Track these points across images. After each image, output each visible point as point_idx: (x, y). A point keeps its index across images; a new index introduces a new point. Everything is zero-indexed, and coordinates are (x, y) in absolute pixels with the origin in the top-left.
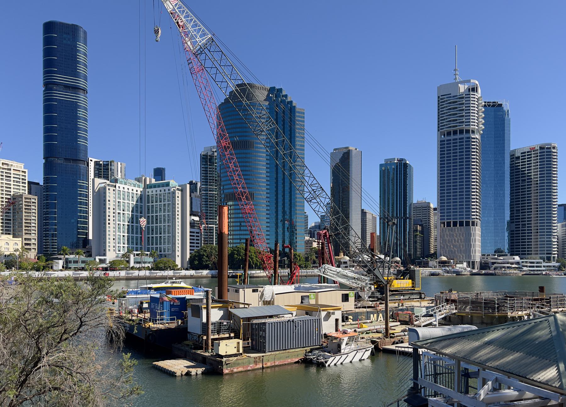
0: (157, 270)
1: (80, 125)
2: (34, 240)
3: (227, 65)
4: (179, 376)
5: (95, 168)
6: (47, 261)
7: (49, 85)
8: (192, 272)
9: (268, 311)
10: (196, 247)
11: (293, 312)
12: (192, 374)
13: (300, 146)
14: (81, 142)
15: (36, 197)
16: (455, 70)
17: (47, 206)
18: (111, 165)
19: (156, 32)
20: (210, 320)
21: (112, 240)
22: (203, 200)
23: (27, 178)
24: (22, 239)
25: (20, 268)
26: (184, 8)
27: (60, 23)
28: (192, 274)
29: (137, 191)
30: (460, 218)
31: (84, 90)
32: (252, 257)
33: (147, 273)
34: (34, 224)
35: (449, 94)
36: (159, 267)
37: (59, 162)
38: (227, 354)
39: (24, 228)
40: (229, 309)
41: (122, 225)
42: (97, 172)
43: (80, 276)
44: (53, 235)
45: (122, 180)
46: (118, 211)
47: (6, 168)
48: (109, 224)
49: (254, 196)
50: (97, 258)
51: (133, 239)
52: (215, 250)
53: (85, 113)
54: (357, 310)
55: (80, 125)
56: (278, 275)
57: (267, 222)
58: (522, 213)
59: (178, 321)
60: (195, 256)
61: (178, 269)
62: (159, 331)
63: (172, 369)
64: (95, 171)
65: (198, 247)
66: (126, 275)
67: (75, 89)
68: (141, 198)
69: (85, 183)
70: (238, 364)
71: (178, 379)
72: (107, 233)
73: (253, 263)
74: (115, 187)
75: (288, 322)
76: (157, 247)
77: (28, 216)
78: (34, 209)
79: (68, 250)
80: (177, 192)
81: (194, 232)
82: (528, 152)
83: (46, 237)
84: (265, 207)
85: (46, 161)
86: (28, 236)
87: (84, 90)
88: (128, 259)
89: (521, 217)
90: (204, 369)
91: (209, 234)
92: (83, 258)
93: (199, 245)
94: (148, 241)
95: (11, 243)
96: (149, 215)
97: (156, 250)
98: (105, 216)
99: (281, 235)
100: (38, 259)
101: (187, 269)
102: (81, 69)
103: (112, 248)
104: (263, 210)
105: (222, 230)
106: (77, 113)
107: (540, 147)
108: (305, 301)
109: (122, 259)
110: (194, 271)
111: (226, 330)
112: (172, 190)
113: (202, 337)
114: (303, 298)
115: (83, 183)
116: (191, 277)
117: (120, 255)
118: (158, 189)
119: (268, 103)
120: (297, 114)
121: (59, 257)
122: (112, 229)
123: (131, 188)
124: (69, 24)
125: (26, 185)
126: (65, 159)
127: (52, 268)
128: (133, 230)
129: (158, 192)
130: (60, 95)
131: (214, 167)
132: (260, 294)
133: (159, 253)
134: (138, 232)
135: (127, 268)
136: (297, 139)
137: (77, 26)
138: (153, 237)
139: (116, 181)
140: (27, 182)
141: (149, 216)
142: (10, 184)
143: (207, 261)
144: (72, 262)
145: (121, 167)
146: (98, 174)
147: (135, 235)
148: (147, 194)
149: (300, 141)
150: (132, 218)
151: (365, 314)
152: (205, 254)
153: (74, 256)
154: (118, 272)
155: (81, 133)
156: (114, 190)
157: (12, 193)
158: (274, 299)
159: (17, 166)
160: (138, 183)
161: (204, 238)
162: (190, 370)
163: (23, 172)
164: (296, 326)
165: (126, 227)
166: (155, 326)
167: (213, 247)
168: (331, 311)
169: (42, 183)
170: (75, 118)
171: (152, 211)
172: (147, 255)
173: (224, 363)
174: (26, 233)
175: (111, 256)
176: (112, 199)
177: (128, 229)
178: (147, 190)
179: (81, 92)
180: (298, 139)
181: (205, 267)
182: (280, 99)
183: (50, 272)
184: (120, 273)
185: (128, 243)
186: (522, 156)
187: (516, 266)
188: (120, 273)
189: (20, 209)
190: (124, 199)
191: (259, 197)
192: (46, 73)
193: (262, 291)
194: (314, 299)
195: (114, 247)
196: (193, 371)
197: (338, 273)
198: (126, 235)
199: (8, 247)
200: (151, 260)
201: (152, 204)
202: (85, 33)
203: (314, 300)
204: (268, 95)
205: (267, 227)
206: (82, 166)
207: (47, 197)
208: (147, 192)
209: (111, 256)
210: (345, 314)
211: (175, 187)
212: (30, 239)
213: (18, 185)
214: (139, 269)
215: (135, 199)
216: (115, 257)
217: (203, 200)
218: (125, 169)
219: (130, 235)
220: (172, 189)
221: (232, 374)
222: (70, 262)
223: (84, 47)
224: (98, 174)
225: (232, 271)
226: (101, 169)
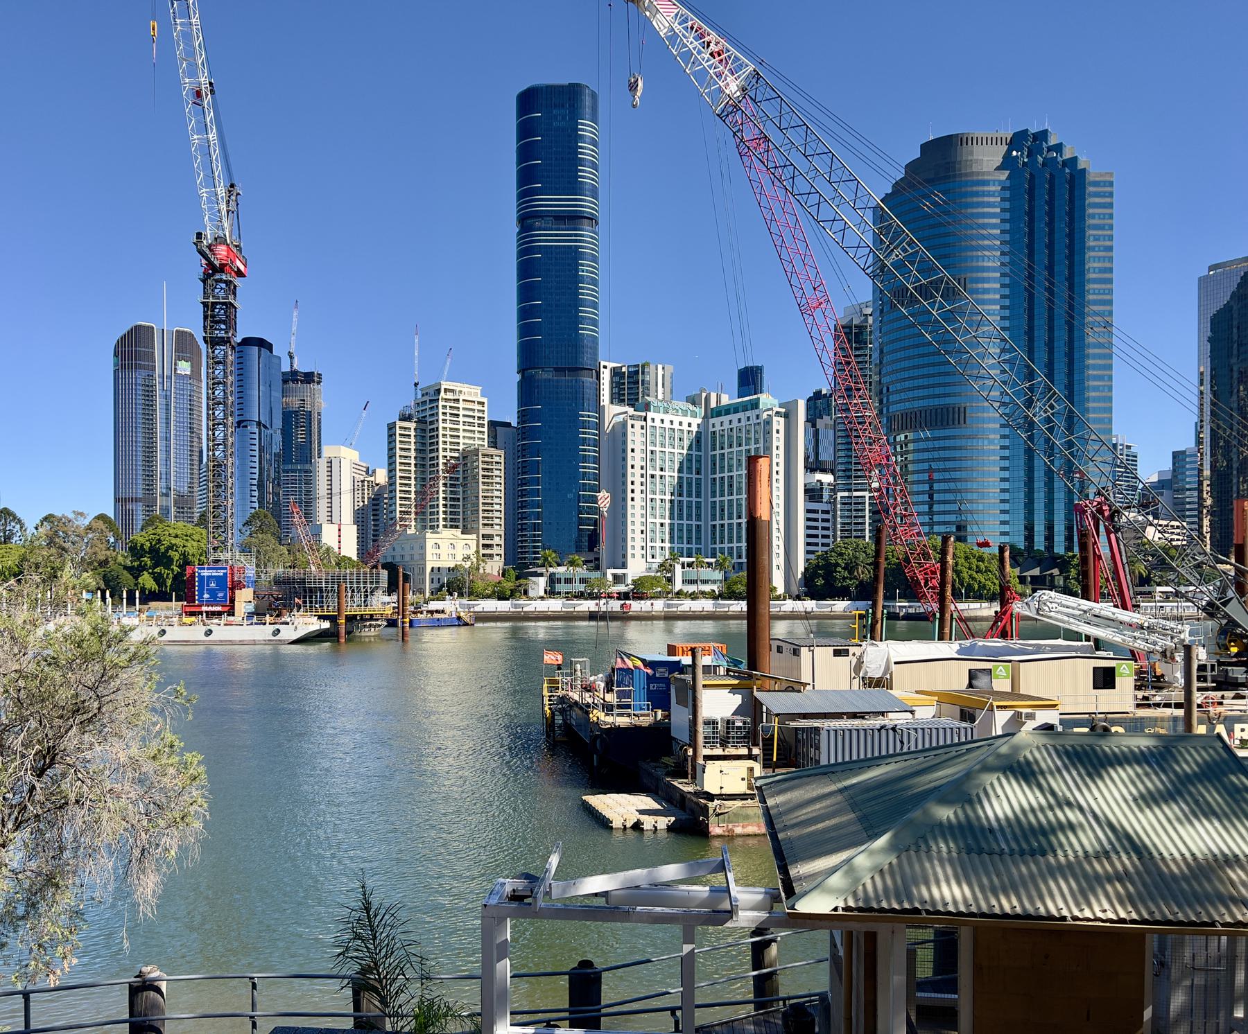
0: (730, 598)
1: (583, 294)
2: (498, 538)
3: (793, 124)
4: (620, 829)
5: (612, 382)
6: (518, 578)
7: (527, 221)
8: (810, 605)
9: (873, 699)
10: (823, 545)
11: (914, 708)
12: (645, 827)
13: (1100, 272)
14: (586, 330)
15: (502, 453)
17: (525, 468)
18: (643, 373)
19: (633, 87)
20: (699, 714)
21: (638, 535)
22: (840, 434)
23: (486, 415)
24: (478, 537)
25: (471, 594)
26: (692, 20)
27: (547, 87)
28: (809, 610)
29: (690, 425)
31: (592, 219)
32: (959, 568)
33: (707, 605)
34: (499, 505)
36: (734, 592)
37: (545, 376)
38: (724, 791)
39: (481, 515)
40: (756, 693)
41: (658, 502)
42: (617, 390)
43: (525, 609)
44: (535, 527)
45: (660, 404)
46: (650, 472)
47: (452, 397)
48: (633, 499)
49: (967, 415)
50: (610, 572)
51: (680, 530)
52: (865, 552)
53: (593, 267)
54: (1142, 713)
55: (583, 294)
56: (952, 615)
57: (1003, 480)
59: (656, 712)
60: (817, 566)
61: (778, 598)
62: (616, 731)
63: (608, 813)
64: (611, 389)
65: (828, 545)
66: (665, 609)
67: (574, 219)
68: (698, 440)
69: (593, 417)
70: (747, 817)
71: (617, 835)
72: (630, 519)
73: (962, 584)
74: (645, 420)
75: (879, 730)
76: (732, 548)
77: (488, 490)
78: (499, 474)
79: (552, 556)
80: (775, 419)
81: (816, 512)
83: (522, 530)
84: (996, 441)
85: (523, 377)
86: (488, 531)
87: (592, 219)
88: (669, 575)
90: (673, 819)
91: (854, 514)
92: (582, 572)
93: (830, 541)
94: (714, 534)
95: (460, 545)
96: (714, 476)
97: (729, 553)
98: (624, 483)
99: (1043, 512)
100: (503, 575)
101: (798, 598)
102: (586, 175)
103: (638, 552)
104: (992, 447)
105: (755, 511)
106: (577, 270)
108: (982, 682)
109: (659, 574)
110: (814, 602)
111: (741, 738)
112: (765, 416)
113: (686, 750)
114: (972, 675)
115: (589, 416)
116: (807, 616)
117: (655, 566)
118: (734, 417)
119: (1007, 173)
120: (1091, 189)
121: (539, 570)
122: (638, 511)
123: (676, 419)
124: (562, 87)
125: (485, 429)
126: (557, 370)
127: (526, 592)
128: (680, 510)
129: (735, 424)
130: (548, 237)
131: (868, 352)
132: (854, 661)
133: (735, 560)
134: (691, 515)
135: (668, 593)
136: (1090, 254)
137: (578, 85)
138: (723, 526)
139: (647, 407)
140: (486, 423)
141: (714, 479)
142: (458, 430)
143: (844, 578)
144: (563, 581)
145: (663, 375)
146: (617, 398)
147: (685, 522)
148: (711, 429)
149: (1099, 257)
150: (680, 485)
151: (1166, 724)
152: (840, 561)
153: (565, 568)
154: (649, 602)
155: (586, 312)
156: (642, 428)
157: (461, 447)
158: (891, 675)
159: (470, 393)
160: (691, 407)
161: (842, 523)
162: (644, 818)
163: (479, 403)
164: (902, 742)
165: (668, 505)
166: (609, 719)
167: (861, 546)
168: (1024, 711)
169: (514, 424)
170: (574, 280)
171: (720, 467)
172: (709, 564)
173: (711, 811)
174: (485, 525)
175: (636, 568)
176: (638, 447)
177: (671, 509)
178: (712, 421)
179: (586, 225)
180: (1092, 254)
181: (842, 594)
182: (1040, 159)
183: (521, 602)
184: (652, 604)
185: (671, 541)
188: (652, 604)
189: (475, 476)
190: (662, 445)
191: (980, 415)
192: (521, 195)
193: (858, 654)
194: (1005, 678)
195: (642, 548)
196: (648, 822)
197: (1085, 612)
198: (667, 521)
199: (438, 551)
200: (718, 575)
201: (722, 451)
202: (594, 96)
203: (1008, 682)
204: (1007, 156)
205: (1003, 490)
206: (588, 380)
207: (524, 451)
208: (711, 426)
209: (636, 568)
210: (1100, 720)
211: (772, 409)
212: (490, 537)
213: (471, 431)
214: (693, 596)
215: (686, 443)
216: (644, 570)
217: (840, 434)
218: (671, 377)
219: (676, 522)
220: (766, 413)
221: (730, 837)
222: (559, 581)
223: (591, 127)
224: (617, 398)
225: (907, 604)
226: (624, 384)
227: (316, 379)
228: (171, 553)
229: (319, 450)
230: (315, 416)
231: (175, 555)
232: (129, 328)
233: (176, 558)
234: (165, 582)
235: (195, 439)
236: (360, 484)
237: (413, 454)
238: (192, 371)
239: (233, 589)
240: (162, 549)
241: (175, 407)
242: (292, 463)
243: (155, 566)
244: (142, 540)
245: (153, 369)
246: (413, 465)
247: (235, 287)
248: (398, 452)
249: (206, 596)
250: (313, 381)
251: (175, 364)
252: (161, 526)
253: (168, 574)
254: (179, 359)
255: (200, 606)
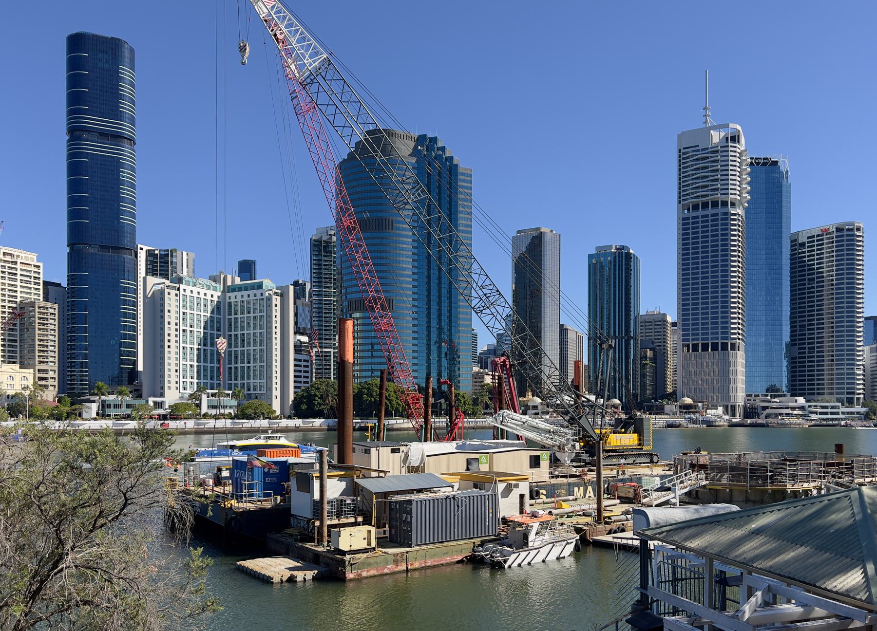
0: (243, 418)
1: (124, 193)
2: (52, 373)
3: (351, 100)
4: (278, 583)
5: (147, 260)
6: (72, 404)
7: (75, 132)
8: (298, 422)
9: (415, 482)
10: (304, 382)
11: (453, 484)
12: (298, 579)
13: (465, 227)
14: (126, 220)
15: (56, 306)
16: (705, 109)
17: (74, 319)
18: (172, 256)
19: (242, 49)
20: (325, 497)
21: (173, 373)
22: (314, 310)
23: (41, 276)
24: (34, 371)
25: (31, 416)
26: (284, 12)
27: (94, 36)
28: (298, 425)
29: (212, 296)
30: (712, 339)
31: (131, 140)
32: (391, 398)
33: (228, 423)
34: (53, 347)
35: (695, 146)
36: (246, 414)
37: (92, 250)
38: (352, 548)
39: (37, 354)
40: (356, 480)
41: (189, 349)
42: (151, 267)
43: (125, 427)
44: (82, 365)
45: (189, 279)
46: (182, 328)
47: (10, 260)
48: (169, 347)
49: (394, 304)
50: (151, 401)
51: (205, 370)
52: (333, 387)
53: (132, 175)
54: (554, 481)
55: (124, 193)
56: (431, 426)
57: (414, 345)
58: (809, 330)
59: (276, 498)
60: (302, 396)
61: (276, 418)
62: (247, 513)
63: (267, 573)
64: (147, 265)
65: (307, 382)
66: (195, 427)
67: (117, 137)
68: (218, 308)
69: (132, 284)
70: (369, 564)
71: (276, 587)
72: (167, 361)
73: (393, 408)
74: (179, 289)
75: (446, 499)
76: (244, 384)
77: (43, 335)
78: (53, 324)
79: (105, 387)
80: (274, 297)
81: (300, 360)
82: (818, 236)
83: (71, 367)
84: (410, 322)
85: (72, 249)
86: (43, 367)
87: (131, 140)
88: (198, 402)
89: (807, 337)
90: (316, 571)
91: (324, 363)
92: (128, 399)
93: (309, 380)
94: (230, 374)
95: (18, 377)
96: (230, 333)
97: (241, 387)
98: (163, 335)
99: (436, 365)
100: (59, 401)
101: (290, 417)
102: (126, 107)
103: (173, 385)
104: (408, 325)
105: (344, 356)
106: (119, 176)
107: (836, 228)
108: (473, 467)
109: (190, 401)
110: (301, 420)
111: (350, 511)
112: (267, 294)
113: (313, 523)
114: (469, 462)
115: (129, 284)
116: (296, 429)
117: (186, 396)
118: (245, 293)
119: (415, 159)
120: (460, 177)
121: (92, 398)
122: (173, 356)
123: (202, 292)
124: (106, 38)
125: (41, 287)
126: (101, 247)
127: (80, 415)
128: (205, 356)
129: (245, 298)
130: (93, 147)
131: (332, 259)
132: (403, 455)
133: (246, 392)
134: (214, 360)
135: (197, 415)
136: (460, 215)
137: (119, 40)
138: (237, 368)
139: (180, 280)
140: (41, 282)
141: (231, 335)
142: (15, 286)
143: (320, 405)
144: (112, 406)
145: (187, 259)
146: (152, 271)
147: (209, 365)
148: (228, 300)
149: (465, 218)
150: (205, 338)
151: (565, 487)
152: (317, 393)
153: (115, 396)
154: (183, 422)
155: (126, 207)
156: (176, 295)
157: (18, 300)
158: (424, 464)
159: (27, 258)
160: (213, 284)
161: (317, 369)
162: (295, 573)
163: (35, 266)
164: (458, 506)
165: (196, 352)
166: (241, 505)
167: (331, 384)
168: (514, 482)
169: (64, 284)
170: (117, 183)
171: (235, 327)
172: (228, 395)
173: (347, 563)
174: (40, 362)
175: (171, 397)
176: (173, 309)
177: (199, 355)
178: (228, 295)
179: (126, 143)
180: (461, 215)
181: (318, 414)
182: (433, 154)
183: (77, 422)
184: (185, 423)
185: (199, 377)
186: (808, 242)
187: (800, 412)
188: (185, 423)
189: (31, 323)
190: (191, 309)
191: (401, 305)
192: (71, 112)
193: (405, 451)
194: (486, 463)
195: (177, 382)
196: (300, 576)
197: (524, 423)
198: (195, 364)
199: (12, 382)
200: (235, 402)
201: (236, 316)
202: (132, 51)
203: (487, 465)
204: (415, 148)
205: (414, 351)
206: (128, 257)
207: (73, 306)
208: (227, 298)
209: (171, 397)
210: (534, 487)
211: (271, 290)
212: (46, 371)
213: (28, 287)
214: (216, 417)
215: (209, 309)
216: (178, 398)
217: (314, 310)
218: (194, 262)
219: (202, 364)
220: (267, 293)
221: (359, 580)
222: (109, 406)
223: (130, 73)
224: (152, 271)
225: (359, 421)
226: (157, 262)
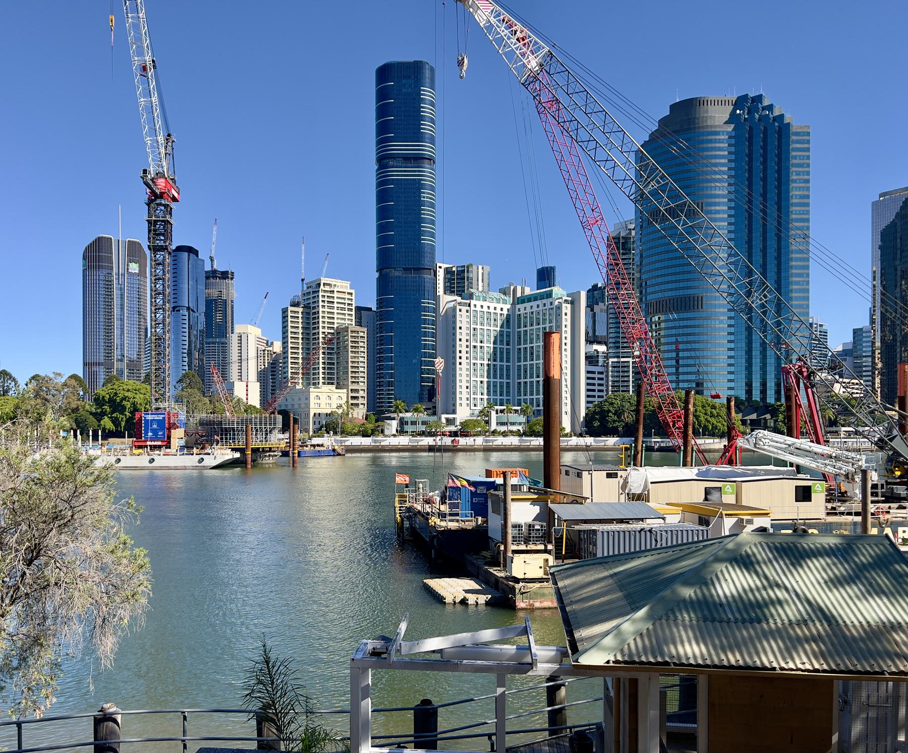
0: (531, 436)
1: (424, 214)
2: (362, 392)
3: (577, 90)
4: (451, 603)
5: (445, 278)
6: (377, 421)
7: (383, 161)
8: (589, 440)
9: (635, 509)
10: (599, 397)
11: (665, 516)
12: (469, 602)
13: (800, 198)
14: (426, 240)
15: (365, 330)
17: (382, 341)
18: (468, 272)
19: (460, 63)
20: (509, 520)
21: (464, 390)
22: (611, 316)
23: (353, 303)
24: (348, 391)
25: (342, 433)
26: (503, 14)
27: (398, 63)
28: (589, 444)
29: (502, 309)
31: (430, 160)
32: (698, 413)
33: (514, 441)
34: (363, 368)
36: (534, 431)
37: (397, 274)
38: (527, 576)
39: (350, 375)
40: (550, 505)
41: (479, 366)
42: (449, 284)
43: (382, 444)
44: (390, 384)
45: (480, 294)
46: (473, 344)
47: (329, 289)
48: (460, 364)
49: (704, 302)
50: (444, 417)
51: (495, 386)
52: (629, 402)
53: (431, 194)
54: (831, 519)
55: (424, 214)
56: (692, 448)
57: (729, 349)
59: (477, 519)
60: (595, 412)
61: (566, 435)
62: (448, 532)
63: (442, 592)
64: (445, 283)
65: (602, 397)
66: (484, 444)
67: (418, 159)
68: (508, 321)
69: (431, 303)
70: (543, 595)
71: (449, 608)
72: (458, 378)
73: (700, 426)
74: (469, 306)
75: (640, 532)
76: (533, 399)
77: (355, 357)
78: (363, 345)
79: (402, 405)
80: (564, 305)
81: (593, 373)
83: (380, 386)
84: (725, 322)
85: (380, 274)
86: (355, 387)
87: (431, 159)
88: (487, 419)
90: (490, 596)
91: (621, 374)
92: (423, 416)
93: (604, 394)
94: (519, 389)
95: (335, 397)
96: (520, 347)
97: (530, 403)
98: (454, 352)
99: (758, 373)
100: (366, 419)
101: (581, 435)
102: (427, 128)
103: (464, 402)
104: (722, 326)
105: (550, 372)
106: (420, 197)
108: (714, 497)
109: (479, 418)
110: (592, 438)
111: (539, 537)
112: (556, 303)
113: (499, 546)
114: (708, 491)
115: (428, 303)
116: (587, 448)
117: (477, 412)
118: (534, 304)
119: (733, 126)
120: (794, 138)
121: (392, 415)
122: (464, 372)
123: (492, 305)
124: (409, 63)
125: (353, 313)
126: (405, 269)
127: (382, 431)
128: (495, 371)
129: (535, 309)
130: (399, 173)
131: (631, 256)
132: (622, 481)
133: (535, 408)
134: (503, 375)
135: (486, 432)
136: (793, 185)
137: (421, 62)
138: (526, 383)
139: (471, 296)
140: (353, 308)
141: (520, 349)
142: (333, 313)
143: (614, 421)
144: (409, 423)
145: (483, 273)
146: (449, 290)
147: (498, 380)
148: (517, 313)
149: (800, 187)
150: (495, 353)
151: (848, 527)
152: (611, 409)
153: (411, 414)
154: (472, 439)
155: (426, 227)
156: (467, 311)
157: (335, 326)
158: (648, 491)
159: (342, 287)
160: (503, 296)
161: (612, 381)
162: (469, 596)
163: (349, 293)
164: (656, 541)
165: (486, 368)
166: (443, 524)
167: (627, 398)
168: (745, 518)
169: (374, 309)
170: (418, 204)
171: (524, 340)
172: (516, 411)
173: (517, 591)
174: (353, 382)
175: (463, 414)
176: (464, 326)
177: (489, 371)
178: (518, 306)
179: (426, 164)
180: (794, 185)
181: (613, 432)
182: (757, 116)
183: (379, 438)
184: (474, 440)
185: (488, 394)
188: (474, 440)
189: (345, 347)
190: (482, 324)
191: (713, 302)
192: (379, 142)
193: (624, 476)
194: (732, 493)
195: (467, 399)
196: (472, 599)
197: (789, 445)
198: (485, 380)
199: (318, 401)
200: (522, 419)
201: (525, 329)
202: (432, 70)
203: (734, 497)
204: (733, 113)
205: (730, 357)
206: (428, 277)
207: (381, 328)
208: (517, 310)
209: (463, 414)
210: (800, 524)
211: (561, 298)
212: (357, 391)
213: (343, 314)
214: (504, 434)
215: (499, 323)
216: (468, 415)
217: (611, 316)
218: (489, 275)
219: (492, 380)
220: (557, 301)
221: (531, 610)
222: (407, 423)
223: (430, 92)
224: (449, 290)
225: (660, 440)
226: (454, 279)
227: (230, 276)
228: (124, 403)
229: (232, 328)
230: (229, 303)
231: (127, 404)
232: (94, 239)
233: (128, 406)
234: (120, 424)
235: (142, 320)
236: (262, 352)
237: (300, 331)
238: (140, 270)
239: (169, 429)
240: (118, 400)
241: (128, 297)
242: (213, 337)
243: (113, 412)
244: (103, 393)
245: (112, 268)
246: (300, 339)
247: (171, 209)
248: (290, 330)
249: (150, 434)
250: (228, 278)
251: (128, 265)
252: (117, 383)
253: (122, 418)
254: (130, 261)
255: (145, 441)
